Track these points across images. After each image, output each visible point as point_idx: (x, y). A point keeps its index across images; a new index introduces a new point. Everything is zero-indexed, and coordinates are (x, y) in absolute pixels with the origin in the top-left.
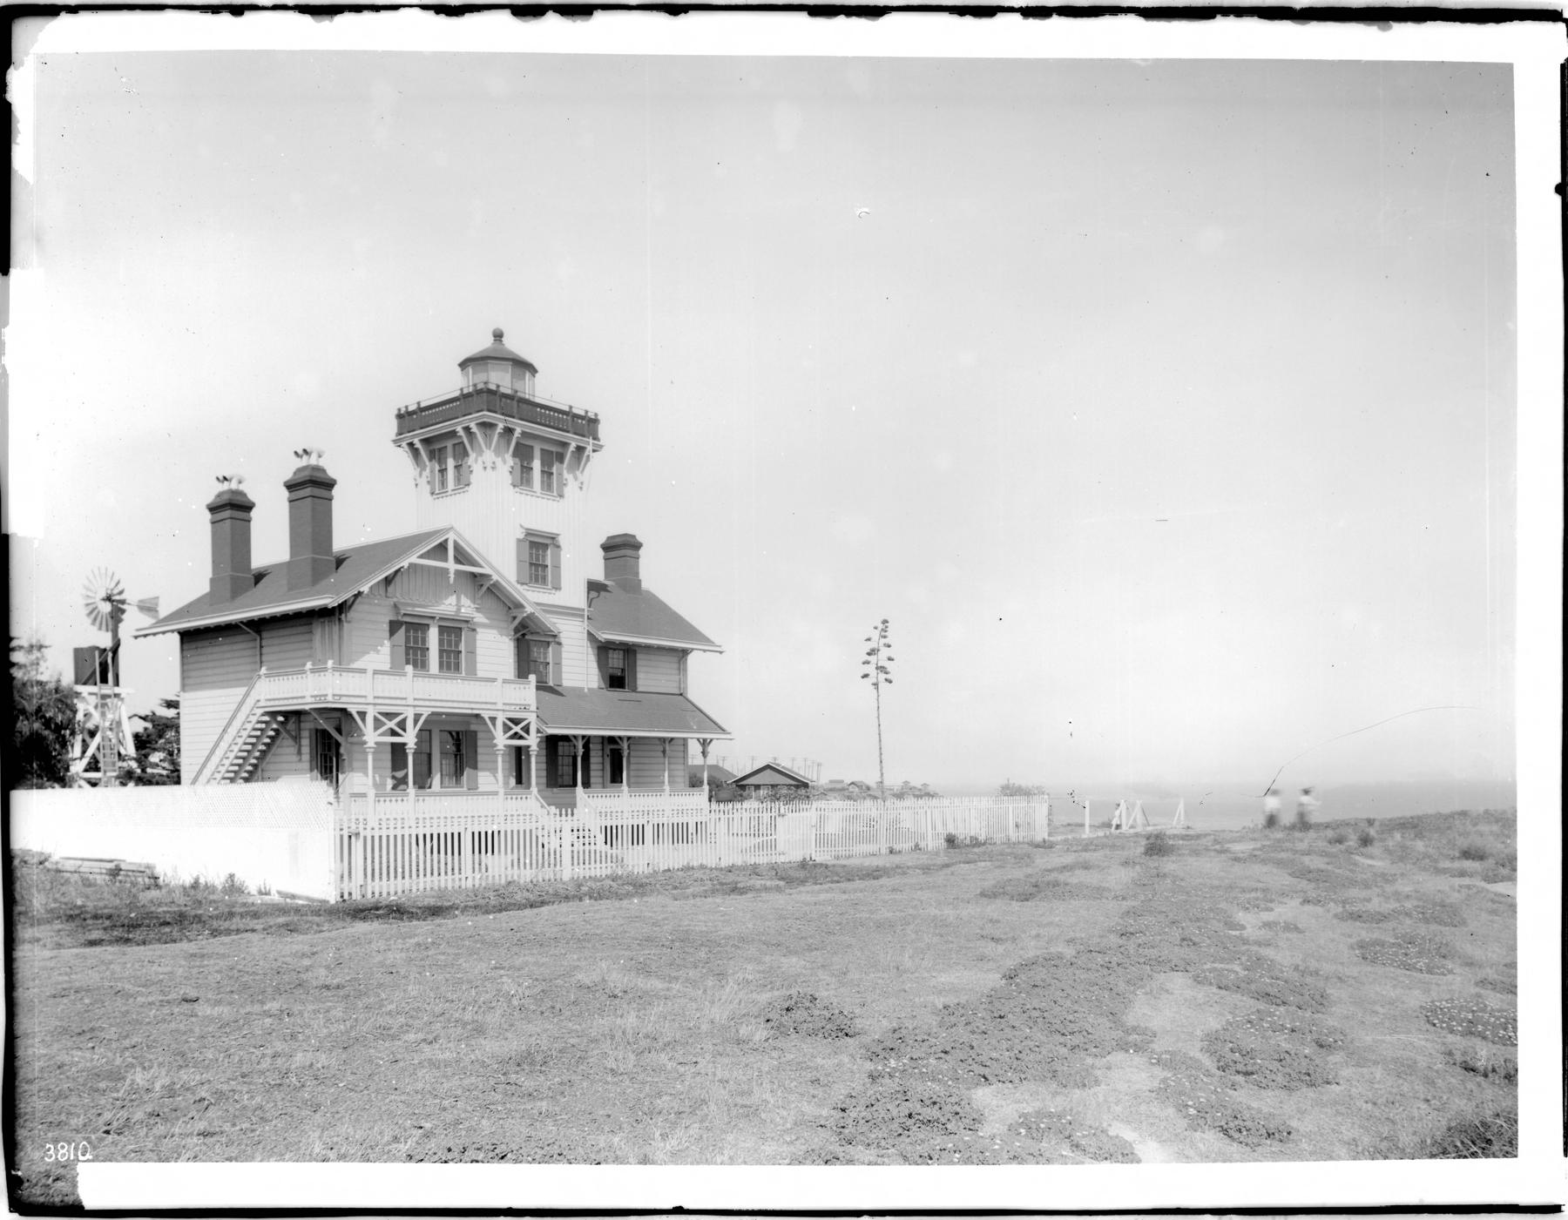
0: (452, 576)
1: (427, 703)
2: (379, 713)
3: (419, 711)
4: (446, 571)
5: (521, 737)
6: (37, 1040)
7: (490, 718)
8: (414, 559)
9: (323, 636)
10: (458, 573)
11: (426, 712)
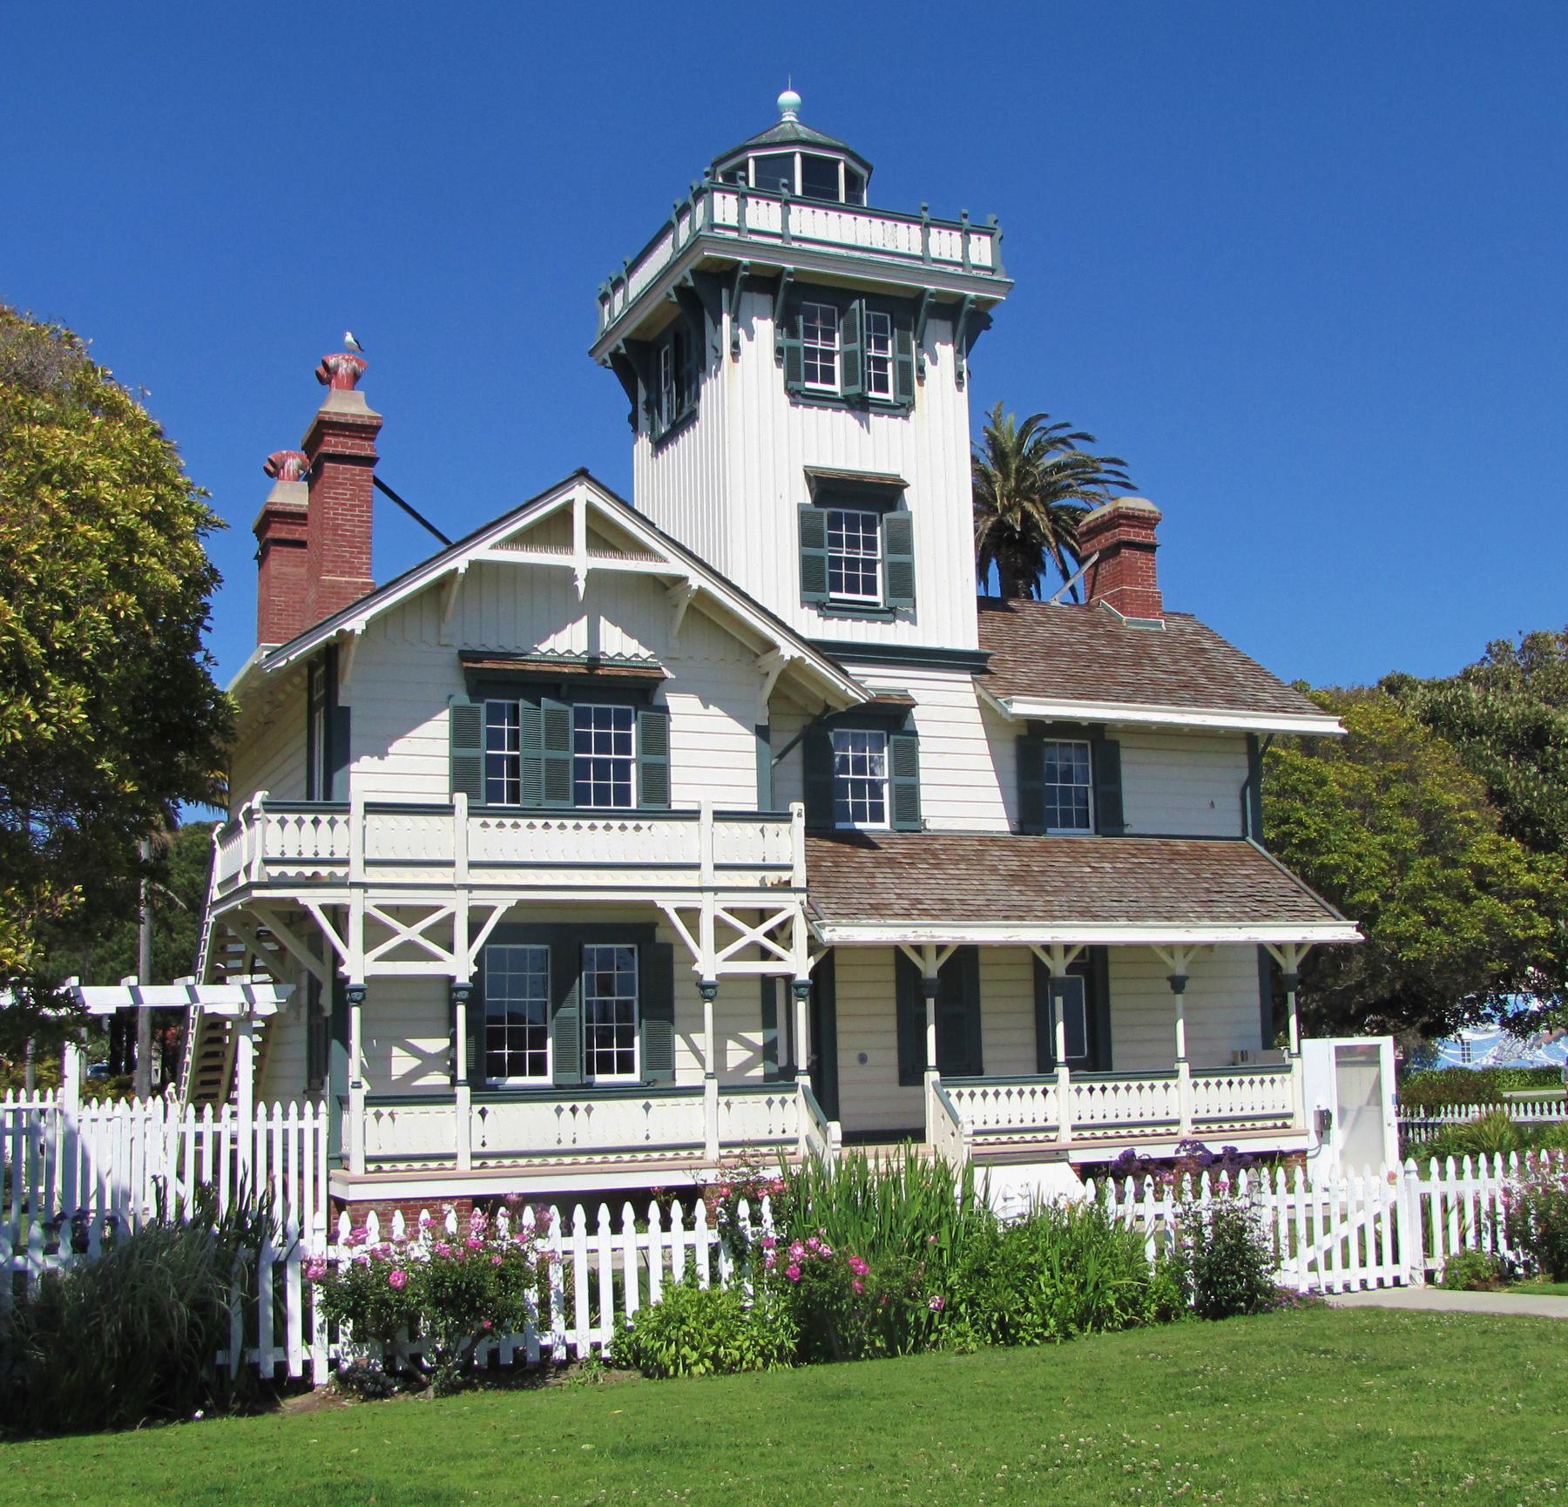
0: (581, 585)
1: (500, 877)
2: (379, 907)
3: (482, 898)
4: (568, 574)
5: (765, 955)
6: (113, 964)
7: (680, 911)
8: (482, 551)
9: (160, 1320)
10: (593, 575)
11: (503, 903)
